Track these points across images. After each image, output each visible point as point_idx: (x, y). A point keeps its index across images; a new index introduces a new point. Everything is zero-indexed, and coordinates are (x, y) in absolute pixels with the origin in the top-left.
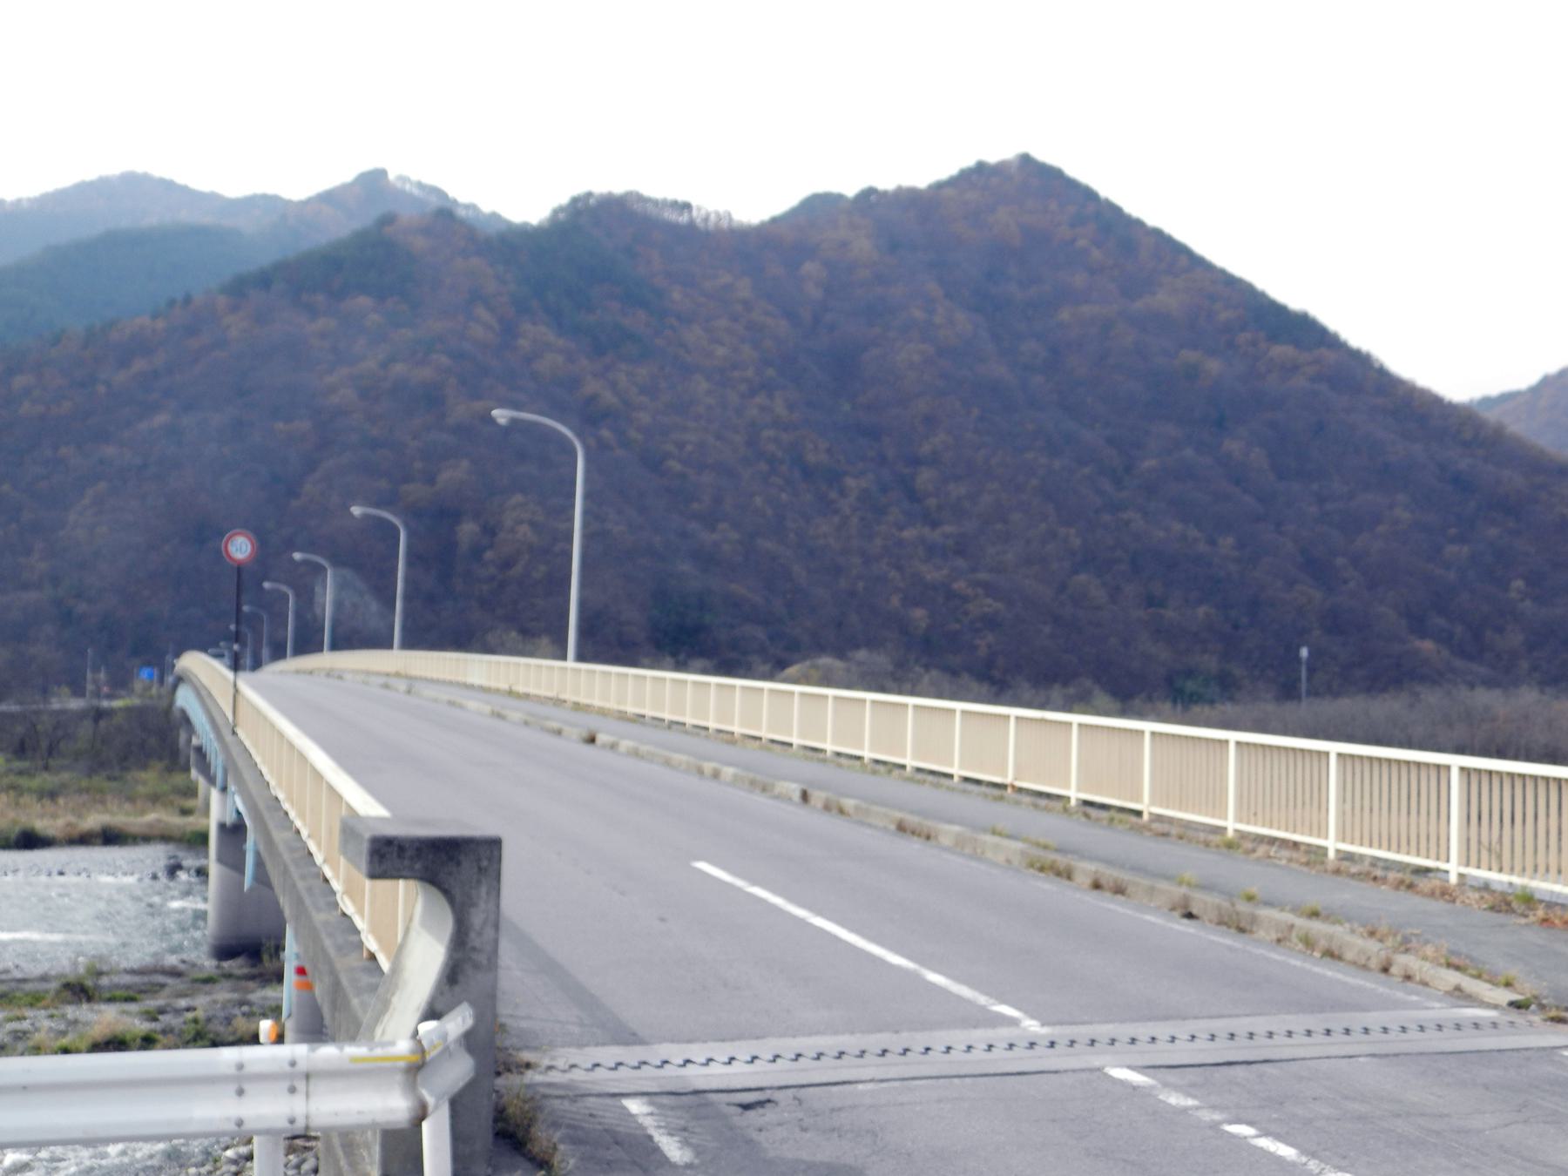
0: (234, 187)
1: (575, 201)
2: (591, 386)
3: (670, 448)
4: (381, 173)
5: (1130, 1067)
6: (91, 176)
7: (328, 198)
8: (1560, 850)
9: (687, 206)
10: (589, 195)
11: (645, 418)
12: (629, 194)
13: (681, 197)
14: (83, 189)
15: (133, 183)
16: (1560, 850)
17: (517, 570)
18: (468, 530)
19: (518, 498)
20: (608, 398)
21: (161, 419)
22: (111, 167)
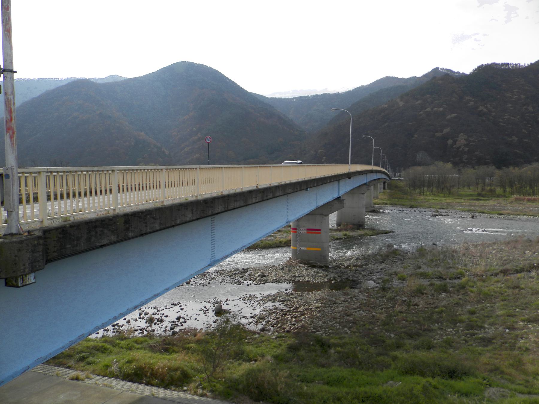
0: (407, 76)
1: (479, 67)
2: (481, 108)
3: (501, 120)
4: (438, 68)
5: (252, 248)
6: (379, 78)
7: (425, 76)
8: (119, 186)
9: (508, 64)
10: (483, 65)
11: (493, 114)
12: (492, 64)
13: (506, 62)
14: (378, 82)
15: (388, 79)
16: (119, 186)
17: (461, 149)
18: (450, 142)
19: (462, 134)
20: (485, 110)
21: (387, 124)
22: (383, 76)
